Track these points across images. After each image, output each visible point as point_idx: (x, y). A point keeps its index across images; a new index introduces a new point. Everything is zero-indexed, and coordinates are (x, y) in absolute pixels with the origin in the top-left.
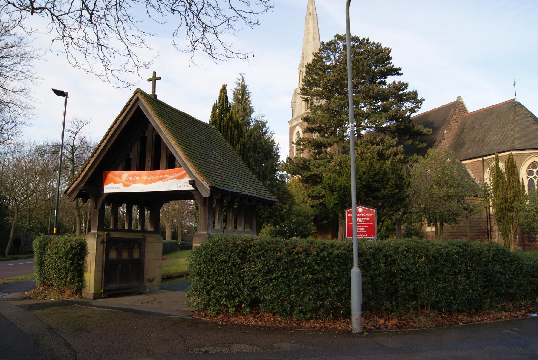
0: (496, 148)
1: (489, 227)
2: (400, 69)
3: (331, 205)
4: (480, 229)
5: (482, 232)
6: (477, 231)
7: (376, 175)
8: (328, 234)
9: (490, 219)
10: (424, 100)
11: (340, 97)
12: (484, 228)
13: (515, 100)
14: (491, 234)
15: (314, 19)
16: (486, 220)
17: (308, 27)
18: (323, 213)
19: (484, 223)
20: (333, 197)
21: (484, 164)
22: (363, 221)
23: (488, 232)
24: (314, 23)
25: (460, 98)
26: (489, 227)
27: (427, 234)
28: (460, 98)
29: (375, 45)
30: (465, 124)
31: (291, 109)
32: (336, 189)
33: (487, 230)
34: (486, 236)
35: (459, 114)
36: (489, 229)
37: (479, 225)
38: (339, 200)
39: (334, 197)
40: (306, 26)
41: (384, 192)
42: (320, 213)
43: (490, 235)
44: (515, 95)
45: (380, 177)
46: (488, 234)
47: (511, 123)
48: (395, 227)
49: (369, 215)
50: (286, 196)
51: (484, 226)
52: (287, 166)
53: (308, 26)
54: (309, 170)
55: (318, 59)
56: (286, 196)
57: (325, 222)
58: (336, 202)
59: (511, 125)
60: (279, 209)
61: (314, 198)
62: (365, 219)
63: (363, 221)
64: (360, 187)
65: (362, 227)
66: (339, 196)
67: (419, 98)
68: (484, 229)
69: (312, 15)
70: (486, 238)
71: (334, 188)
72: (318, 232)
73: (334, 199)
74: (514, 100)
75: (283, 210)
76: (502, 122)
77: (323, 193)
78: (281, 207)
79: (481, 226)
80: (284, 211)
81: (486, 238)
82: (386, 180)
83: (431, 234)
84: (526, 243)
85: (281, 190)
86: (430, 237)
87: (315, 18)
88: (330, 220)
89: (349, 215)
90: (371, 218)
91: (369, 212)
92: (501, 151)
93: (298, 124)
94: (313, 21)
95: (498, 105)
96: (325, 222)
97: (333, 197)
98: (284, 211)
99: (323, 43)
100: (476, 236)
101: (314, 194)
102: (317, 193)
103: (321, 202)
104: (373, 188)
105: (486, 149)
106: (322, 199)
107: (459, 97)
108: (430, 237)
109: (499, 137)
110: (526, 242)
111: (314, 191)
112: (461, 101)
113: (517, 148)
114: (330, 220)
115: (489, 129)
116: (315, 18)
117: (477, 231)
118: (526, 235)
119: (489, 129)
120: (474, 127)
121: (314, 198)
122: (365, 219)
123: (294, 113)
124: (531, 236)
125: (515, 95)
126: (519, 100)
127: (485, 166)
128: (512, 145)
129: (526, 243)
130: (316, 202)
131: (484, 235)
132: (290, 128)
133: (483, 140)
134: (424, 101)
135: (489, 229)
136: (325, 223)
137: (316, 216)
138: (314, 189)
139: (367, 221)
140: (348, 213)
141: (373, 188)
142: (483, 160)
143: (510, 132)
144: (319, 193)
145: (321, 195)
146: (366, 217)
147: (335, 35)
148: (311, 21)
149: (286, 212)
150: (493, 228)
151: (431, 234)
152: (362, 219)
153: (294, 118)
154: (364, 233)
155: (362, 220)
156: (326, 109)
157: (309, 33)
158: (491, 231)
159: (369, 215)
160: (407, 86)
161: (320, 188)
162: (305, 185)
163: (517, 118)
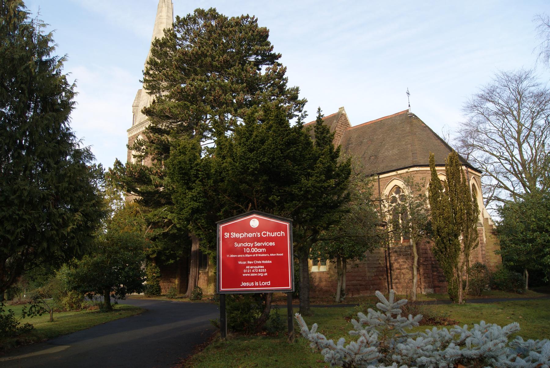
0: (394, 164)
1: (388, 264)
2: (279, 56)
3: (184, 211)
4: (379, 267)
5: (381, 271)
6: (376, 270)
7: (289, 144)
8: (175, 278)
9: (389, 253)
10: (307, 102)
11: (199, 78)
12: (383, 265)
13: (410, 112)
14: (391, 273)
15: (168, 7)
16: (384, 255)
17: (161, 16)
18: (168, 249)
19: (382, 259)
20: (190, 194)
21: (381, 184)
22: (261, 250)
23: (387, 271)
24: (168, 12)
25: (342, 109)
26: (388, 264)
27: (313, 276)
28: (342, 109)
29: (249, 20)
30: (350, 138)
31: (133, 114)
32: (196, 176)
33: (386, 269)
34: (385, 276)
35: (341, 128)
36: (388, 267)
37: (377, 262)
38: (204, 203)
39: (194, 192)
40: (157, 15)
41: (307, 183)
42: (165, 249)
43: (389, 275)
44: (409, 106)
45: (297, 150)
46: (387, 273)
47: (408, 136)
48: (531, 245)
49: (275, 234)
50: (80, 193)
51: (382, 262)
52: (115, 173)
53: (160, 14)
54: (148, 182)
55: (171, 35)
56: (80, 193)
57: (172, 261)
58: (196, 205)
59: (409, 138)
60: (58, 224)
61: (155, 225)
62: (266, 244)
63: (261, 250)
64: (255, 169)
65: (257, 265)
66: (205, 192)
67: (300, 98)
68: (382, 267)
69: (166, 3)
70: (385, 279)
71: (193, 172)
72: (160, 276)
73: (192, 199)
74: (408, 111)
75: (67, 226)
76: (397, 135)
77: (169, 217)
78: (63, 218)
79: (380, 263)
80: (69, 229)
81: (385, 279)
82: (309, 159)
83: (318, 276)
84: (436, 283)
85: (66, 180)
86: (317, 280)
87: (170, 6)
88: (178, 259)
89: (227, 235)
90: (280, 241)
91: (278, 228)
92: (401, 167)
93: (139, 133)
94: (167, 9)
95: (390, 117)
96: (172, 261)
97: (190, 194)
98: (69, 229)
99: (178, 18)
100: (375, 276)
101: (156, 219)
102: (160, 217)
103: (166, 231)
104: (282, 174)
105: (381, 166)
106: (168, 227)
107: (341, 108)
108: (317, 280)
109: (395, 151)
110: (436, 282)
111: (155, 215)
112: (343, 112)
113: (422, 164)
114: (178, 259)
115: (381, 143)
116: (170, 6)
117: (376, 270)
118: (435, 274)
119: (381, 143)
120: (362, 142)
121: (155, 225)
122: (266, 244)
123: (136, 119)
124: (441, 275)
125: (409, 106)
126: (412, 111)
127: (381, 187)
128: (414, 160)
129: (436, 283)
130: (159, 231)
131: (382, 275)
132: (129, 138)
133: (376, 156)
134: (306, 103)
135: (388, 267)
136: (171, 264)
137: (160, 253)
138: (156, 212)
139: (269, 250)
140: (225, 230)
141: (282, 174)
142: (379, 179)
143: (409, 146)
144: (163, 218)
145: (166, 220)
146: (270, 239)
147: (195, 9)
148: (165, 9)
149: (73, 231)
150: (394, 265)
151: (318, 276)
152: (259, 244)
153: (134, 125)
154: (264, 279)
155: (258, 247)
156: (179, 93)
157: (161, 23)
158: (391, 270)
159: (275, 234)
160: (287, 82)
161: (165, 211)
162: (144, 208)
163: (415, 130)
